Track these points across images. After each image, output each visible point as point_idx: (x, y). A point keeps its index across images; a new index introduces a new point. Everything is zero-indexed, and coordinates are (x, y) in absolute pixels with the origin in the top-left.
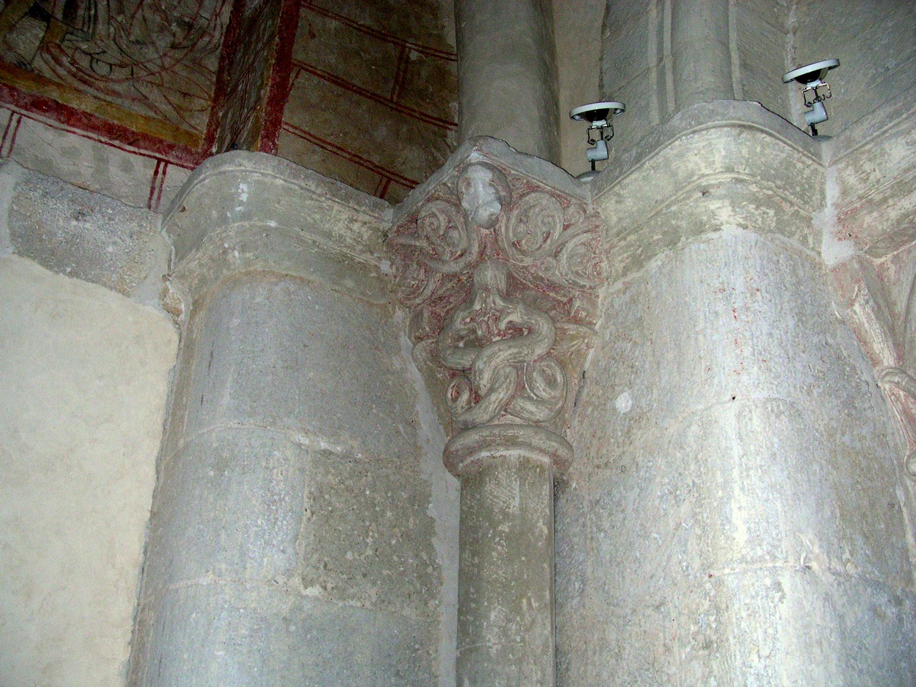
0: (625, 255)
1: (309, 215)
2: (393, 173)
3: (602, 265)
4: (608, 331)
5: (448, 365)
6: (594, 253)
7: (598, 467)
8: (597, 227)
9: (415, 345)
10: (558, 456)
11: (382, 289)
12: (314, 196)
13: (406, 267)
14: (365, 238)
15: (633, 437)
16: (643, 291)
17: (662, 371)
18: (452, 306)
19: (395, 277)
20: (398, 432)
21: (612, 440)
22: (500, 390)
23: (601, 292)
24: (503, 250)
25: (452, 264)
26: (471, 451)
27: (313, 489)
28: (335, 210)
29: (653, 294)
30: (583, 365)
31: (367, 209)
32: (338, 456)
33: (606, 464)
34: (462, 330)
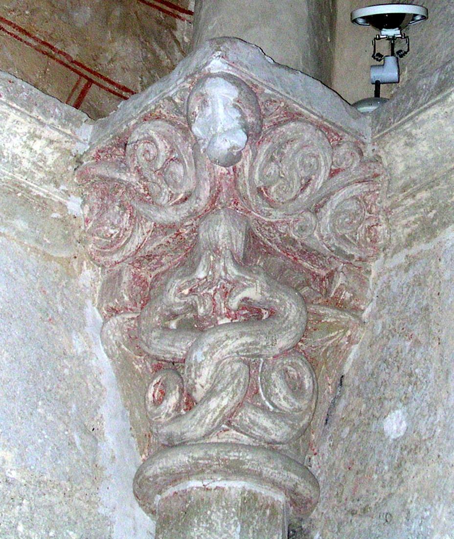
0: (412, 218)
2: (95, 73)
4: (380, 322)
5: (152, 353)
6: (370, 212)
9: (106, 320)
13: (104, 208)
14: (50, 162)
15: (405, 474)
16: (433, 270)
18: (164, 268)
19: (87, 221)
20: (72, 443)
22: (224, 394)
23: (374, 267)
25: (170, 210)
28: (10, 120)
30: (341, 367)
31: (56, 122)
33: (365, 510)
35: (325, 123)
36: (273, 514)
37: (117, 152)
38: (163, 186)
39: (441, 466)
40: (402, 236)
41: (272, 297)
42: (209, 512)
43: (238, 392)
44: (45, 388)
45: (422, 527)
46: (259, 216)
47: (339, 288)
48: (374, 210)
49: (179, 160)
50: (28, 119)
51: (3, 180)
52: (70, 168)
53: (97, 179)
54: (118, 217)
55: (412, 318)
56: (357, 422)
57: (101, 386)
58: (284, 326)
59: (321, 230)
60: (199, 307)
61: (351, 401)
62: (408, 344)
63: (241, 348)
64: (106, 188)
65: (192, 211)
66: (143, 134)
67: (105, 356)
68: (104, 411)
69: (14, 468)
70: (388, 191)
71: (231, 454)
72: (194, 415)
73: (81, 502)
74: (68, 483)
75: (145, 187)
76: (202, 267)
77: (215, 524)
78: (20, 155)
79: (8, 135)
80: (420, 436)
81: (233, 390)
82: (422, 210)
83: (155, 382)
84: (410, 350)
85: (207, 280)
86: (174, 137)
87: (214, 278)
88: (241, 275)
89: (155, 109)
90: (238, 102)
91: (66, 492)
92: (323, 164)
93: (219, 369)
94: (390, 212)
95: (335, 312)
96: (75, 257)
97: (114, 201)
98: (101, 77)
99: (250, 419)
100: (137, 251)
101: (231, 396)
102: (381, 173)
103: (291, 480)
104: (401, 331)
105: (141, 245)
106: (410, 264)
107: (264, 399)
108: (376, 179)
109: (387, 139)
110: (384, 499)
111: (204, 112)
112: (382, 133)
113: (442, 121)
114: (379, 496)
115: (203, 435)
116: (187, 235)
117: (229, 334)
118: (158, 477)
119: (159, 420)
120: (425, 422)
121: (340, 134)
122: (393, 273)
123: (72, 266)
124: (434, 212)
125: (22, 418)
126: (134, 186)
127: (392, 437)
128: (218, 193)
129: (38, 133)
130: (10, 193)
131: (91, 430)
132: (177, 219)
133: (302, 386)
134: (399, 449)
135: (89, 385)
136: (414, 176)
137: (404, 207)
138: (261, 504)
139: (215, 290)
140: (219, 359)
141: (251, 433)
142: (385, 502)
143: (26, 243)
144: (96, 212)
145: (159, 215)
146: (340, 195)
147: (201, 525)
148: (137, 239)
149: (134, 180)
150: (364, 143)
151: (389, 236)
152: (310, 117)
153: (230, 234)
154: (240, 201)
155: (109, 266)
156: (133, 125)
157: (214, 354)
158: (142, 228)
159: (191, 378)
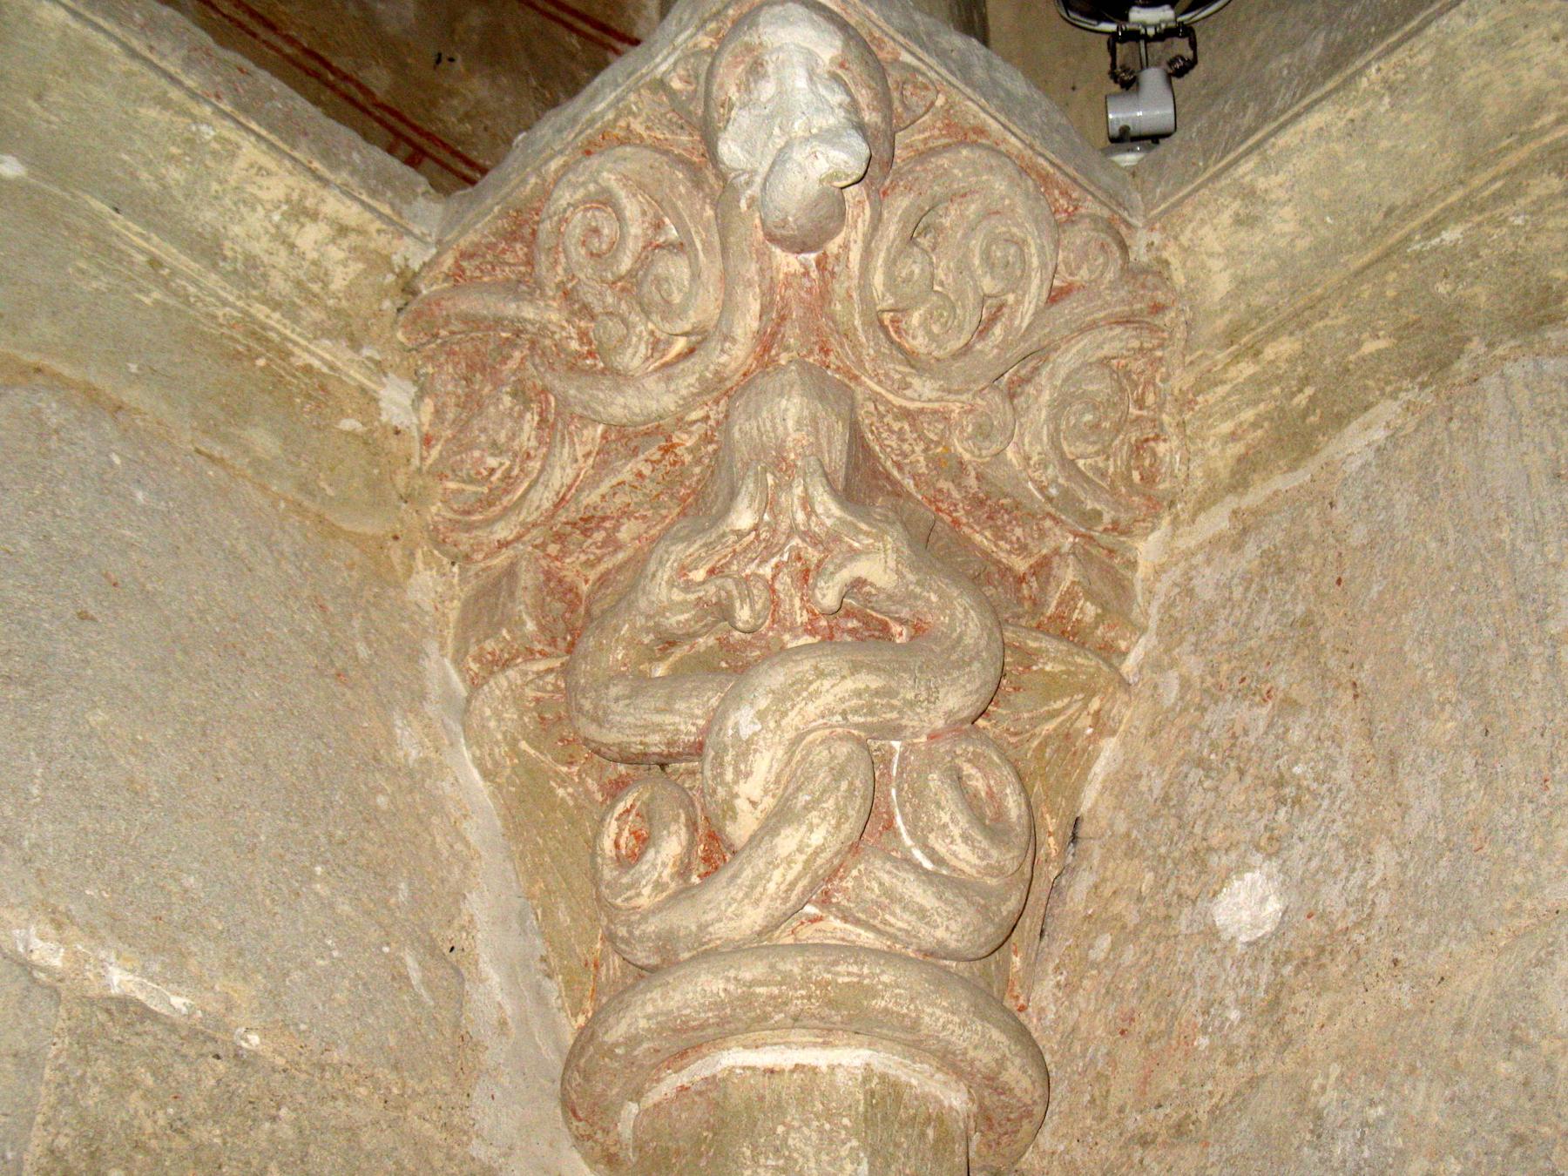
0: (1248, 415)
1: (148, 163)
2: (429, 136)
3: (1161, 448)
4: (1173, 675)
5: (611, 737)
6: (1140, 403)
7: (1145, 1141)
8: (1158, 309)
9: (475, 685)
10: (1002, 1090)
11: (373, 485)
12: (175, 94)
13: (472, 404)
14: (338, 283)
15: (1292, 1022)
16: (1315, 529)
17: (1409, 784)
18: (621, 556)
19: (427, 441)
20: (402, 978)
21: (1203, 1042)
22: (814, 816)
23: (1148, 549)
24: (847, 334)
25: (651, 383)
26: (686, 1041)
27: (62, 1142)
28: (241, 163)
29: (1358, 535)
30: (1075, 794)
31: (354, 182)
32: (173, 1028)
33: (1180, 1130)
34: (672, 607)
35: (1041, 160)
36: (944, 1140)
37: (509, 257)
38: (634, 318)
39: (1406, 986)
40: (1220, 464)
41: (923, 586)
42: (780, 1129)
43: (851, 812)
44: (330, 836)
45: (1365, 1148)
46: (878, 389)
47: (1067, 592)
48: (1150, 399)
49: (679, 247)
50: (288, 164)
51: (221, 320)
52: (387, 304)
53: (456, 326)
54: (509, 424)
55: (1267, 651)
56: (1132, 919)
57: (467, 845)
58: (954, 657)
59: (1026, 440)
60: (738, 604)
61: (1109, 874)
62: (1264, 711)
63: (854, 702)
64: (478, 351)
65: (709, 375)
66: (584, 184)
67: (476, 775)
68: (477, 906)
69: (256, 1024)
70: (1185, 348)
71: (841, 968)
72: (735, 877)
73: (427, 1125)
74: (392, 1076)
75: (583, 336)
76: (746, 502)
77: (801, 1160)
78: (266, 259)
79: (235, 204)
80: (1330, 924)
81: (838, 808)
82: (1276, 390)
83: (620, 808)
84: (1271, 725)
85: (758, 536)
86: (666, 184)
87: (775, 531)
88: (850, 518)
89: (616, 120)
90: (842, 66)
91: (390, 1097)
92: (1035, 262)
93: (798, 757)
94: (1192, 403)
95: (1063, 647)
96: (396, 538)
97: (498, 384)
98: (445, 145)
99: (881, 884)
100: (556, 506)
101: (833, 822)
102: (1169, 302)
103: (992, 1046)
104: (1237, 685)
105: (570, 488)
106: (1245, 531)
107: (908, 841)
108: (1158, 321)
109: (1187, 210)
110: (1238, 1093)
111: (755, 95)
112: (1172, 200)
113: (1338, 148)
114: (1221, 1089)
115: (757, 928)
116: (690, 450)
117: (822, 665)
118: (640, 1043)
119: (634, 903)
120: (1339, 886)
121: (1075, 195)
122: (1200, 558)
123: (388, 557)
124: (1309, 391)
125: (273, 900)
126: (553, 333)
127: (1244, 938)
128: (779, 325)
129: (310, 203)
130: (237, 356)
131: (446, 951)
132: (669, 402)
133: (1000, 814)
134: (1267, 966)
135: (438, 839)
136: (1260, 300)
137: (1228, 387)
138: (912, 1112)
139: (777, 566)
140: (797, 729)
141: (885, 922)
142: (1239, 1100)
143: (274, 488)
144: (450, 416)
145: (620, 400)
146: (1074, 350)
147: (762, 1161)
148: (558, 472)
149: (554, 317)
150: (1129, 225)
151: (1184, 468)
152: (1004, 140)
153: (814, 420)
154: (833, 342)
155: (480, 556)
156: (556, 171)
157: (784, 714)
158: (572, 444)
159: (723, 783)
